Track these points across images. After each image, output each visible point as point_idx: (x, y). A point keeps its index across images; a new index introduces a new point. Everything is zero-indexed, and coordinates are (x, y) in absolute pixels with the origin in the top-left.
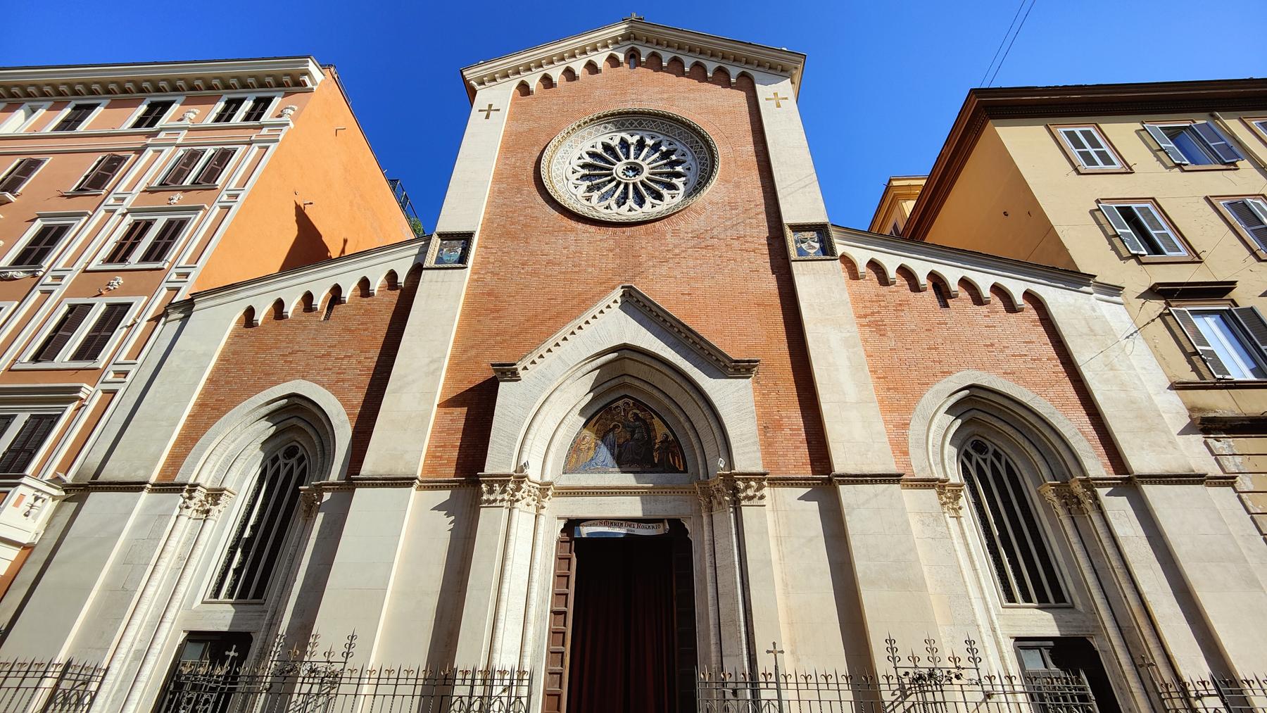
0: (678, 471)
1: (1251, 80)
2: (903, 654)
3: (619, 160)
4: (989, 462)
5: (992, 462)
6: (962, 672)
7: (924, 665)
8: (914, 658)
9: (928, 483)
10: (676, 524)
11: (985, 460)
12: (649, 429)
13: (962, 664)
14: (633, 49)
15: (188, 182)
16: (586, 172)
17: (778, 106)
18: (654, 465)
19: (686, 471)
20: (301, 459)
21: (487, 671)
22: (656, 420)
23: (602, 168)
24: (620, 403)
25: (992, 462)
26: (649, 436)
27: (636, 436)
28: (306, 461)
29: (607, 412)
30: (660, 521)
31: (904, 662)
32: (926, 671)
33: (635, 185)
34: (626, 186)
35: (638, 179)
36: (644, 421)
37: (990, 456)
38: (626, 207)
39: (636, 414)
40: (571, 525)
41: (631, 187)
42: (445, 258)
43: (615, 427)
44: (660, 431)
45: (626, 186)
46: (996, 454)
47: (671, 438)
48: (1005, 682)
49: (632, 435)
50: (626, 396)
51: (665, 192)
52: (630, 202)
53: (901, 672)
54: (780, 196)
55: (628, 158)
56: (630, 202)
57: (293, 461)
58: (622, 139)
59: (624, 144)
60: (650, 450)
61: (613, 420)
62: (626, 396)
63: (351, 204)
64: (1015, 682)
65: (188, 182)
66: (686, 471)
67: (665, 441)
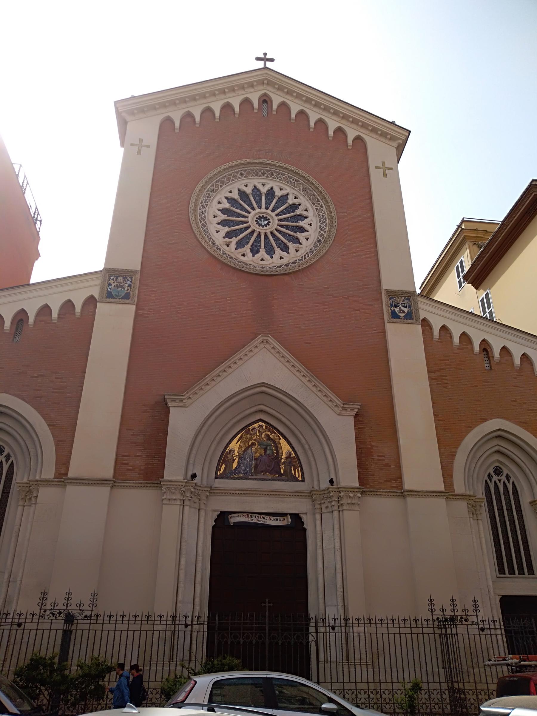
0: (297, 480)
2: (437, 607)
3: (260, 208)
4: (502, 482)
5: (504, 482)
6: (469, 618)
7: (449, 613)
8: (443, 610)
9: (189, 663)
10: (296, 517)
11: (500, 481)
12: (278, 447)
13: (469, 613)
14: (265, 95)
16: (225, 217)
17: (385, 175)
18: (281, 475)
19: (303, 481)
20: (8, 457)
21: (174, 617)
22: (283, 441)
23: (239, 215)
24: (256, 425)
25: (504, 482)
26: (277, 452)
27: (268, 452)
29: (246, 433)
30: (285, 515)
31: (438, 612)
32: (449, 617)
37: (503, 478)
39: (268, 435)
40: (223, 516)
43: (253, 444)
44: (285, 448)
46: (508, 477)
47: (293, 455)
48: (491, 623)
49: (265, 452)
50: (261, 420)
51: (291, 245)
53: (435, 617)
54: (128, 354)
55: (267, 208)
56: (262, 253)
60: (278, 463)
61: (251, 439)
62: (261, 420)
64: (496, 624)
66: (303, 481)
67: (289, 457)
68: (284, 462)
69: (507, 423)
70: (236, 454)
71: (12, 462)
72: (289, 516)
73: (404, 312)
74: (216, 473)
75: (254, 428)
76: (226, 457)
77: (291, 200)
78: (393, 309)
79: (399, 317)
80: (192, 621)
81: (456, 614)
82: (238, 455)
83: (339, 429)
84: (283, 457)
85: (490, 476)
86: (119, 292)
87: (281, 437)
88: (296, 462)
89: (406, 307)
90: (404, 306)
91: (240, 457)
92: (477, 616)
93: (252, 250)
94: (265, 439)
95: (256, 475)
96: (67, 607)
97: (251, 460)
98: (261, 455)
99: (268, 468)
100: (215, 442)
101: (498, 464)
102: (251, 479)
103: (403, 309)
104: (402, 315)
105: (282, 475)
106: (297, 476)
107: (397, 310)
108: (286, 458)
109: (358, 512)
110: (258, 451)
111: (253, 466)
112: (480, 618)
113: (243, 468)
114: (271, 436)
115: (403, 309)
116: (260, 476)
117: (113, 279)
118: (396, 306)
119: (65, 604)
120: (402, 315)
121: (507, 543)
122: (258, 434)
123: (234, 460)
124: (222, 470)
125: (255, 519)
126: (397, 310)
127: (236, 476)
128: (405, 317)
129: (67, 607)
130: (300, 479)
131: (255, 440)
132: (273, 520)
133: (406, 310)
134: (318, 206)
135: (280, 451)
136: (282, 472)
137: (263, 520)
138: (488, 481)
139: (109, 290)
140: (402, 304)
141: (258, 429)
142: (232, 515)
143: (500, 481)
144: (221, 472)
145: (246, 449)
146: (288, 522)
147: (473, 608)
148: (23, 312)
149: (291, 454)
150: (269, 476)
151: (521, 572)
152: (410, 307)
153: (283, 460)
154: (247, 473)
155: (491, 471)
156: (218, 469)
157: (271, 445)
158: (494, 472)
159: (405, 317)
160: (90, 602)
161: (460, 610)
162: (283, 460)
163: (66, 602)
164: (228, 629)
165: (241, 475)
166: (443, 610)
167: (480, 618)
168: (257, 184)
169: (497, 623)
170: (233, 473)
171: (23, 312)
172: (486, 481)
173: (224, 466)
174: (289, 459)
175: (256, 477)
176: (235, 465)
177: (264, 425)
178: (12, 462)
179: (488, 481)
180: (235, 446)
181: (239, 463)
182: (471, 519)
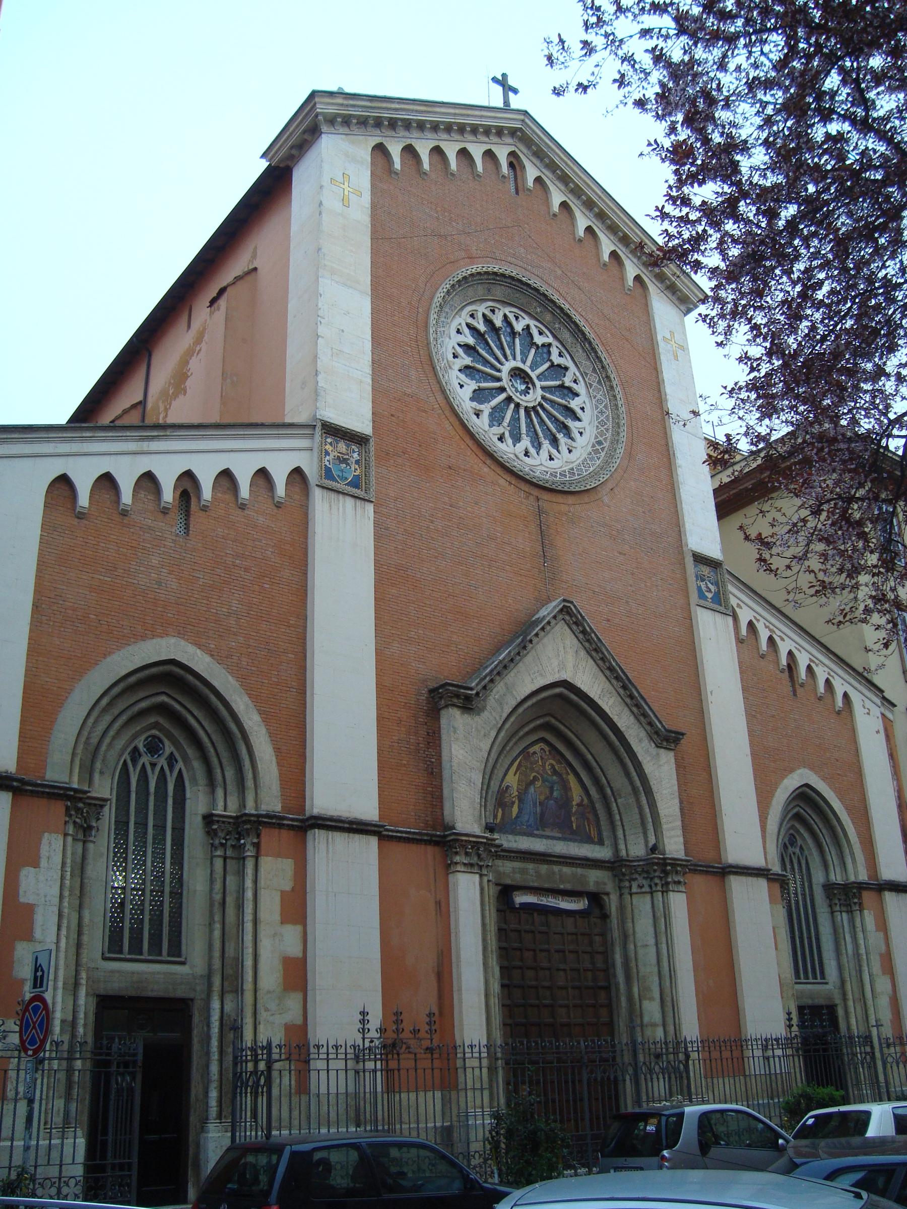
4: (158, 769)
10: (596, 899)
11: (153, 765)
12: (566, 788)
39: (553, 766)
69: (191, 649)
71: (180, 769)
81: (401, 1036)
85: (135, 754)
86: (342, 471)
101: (155, 732)
109: (684, 895)
113: (526, 818)
116: (548, 832)
117: (331, 444)
123: (513, 803)
134: (594, 382)
138: (166, 768)
141: (539, 754)
143: (153, 765)
147: (427, 1028)
148: (188, 476)
154: (530, 826)
155: (140, 744)
158: (145, 746)
164: (595, 1061)
168: (508, 314)
169: (476, 1050)
171: (188, 476)
175: (544, 833)
176: (515, 810)
177: (547, 749)
178: (180, 769)
179: (166, 768)
180: (512, 780)
182: (70, 839)
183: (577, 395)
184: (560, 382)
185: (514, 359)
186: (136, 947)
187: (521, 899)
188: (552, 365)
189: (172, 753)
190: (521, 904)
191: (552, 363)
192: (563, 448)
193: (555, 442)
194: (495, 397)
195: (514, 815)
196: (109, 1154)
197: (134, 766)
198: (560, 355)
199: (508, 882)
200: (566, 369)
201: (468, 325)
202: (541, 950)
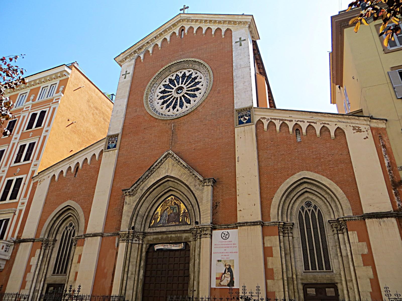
1: (332, 46)
4: (311, 211)
6: (253, 297)
11: (309, 210)
15: (4, 222)
22: (182, 205)
24: (169, 198)
27: (174, 211)
28: (75, 228)
33: (186, 93)
34: (186, 93)
35: (185, 91)
36: (177, 205)
37: (312, 208)
38: (184, 107)
39: (175, 202)
41: (185, 95)
42: (110, 146)
43: (168, 208)
45: (183, 96)
46: (315, 207)
47: (186, 211)
49: (173, 211)
52: (185, 104)
57: (71, 228)
58: (169, 79)
59: (171, 81)
61: (167, 205)
63: (93, 114)
65: (4, 222)
68: (182, 215)
70: (160, 214)
71: (319, 209)
72: (182, 244)
73: (246, 119)
74: (150, 225)
75: (169, 200)
76: (155, 216)
77: (187, 74)
78: (240, 119)
79: (243, 123)
80: (86, 298)
81: (245, 295)
82: (160, 215)
83: (205, 195)
84: (181, 213)
85: (303, 208)
87: (181, 202)
88: (188, 214)
89: (248, 116)
90: (246, 116)
91: (161, 216)
92: (258, 296)
93: (187, 103)
94: (173, 205)
95: (168, 224)
96: (244, 294)
97: (166, 217)
98: (171, 213)
99: (174, 220)
100: (285, 196)
102: (166, 226)
103: (246, 117)
104: (245, 121)
105: (181, 222)
106: (188, 222)
107: (242, 119)
108: (183, 213)
110: (169, 212)
111: (167, 219)
112: (260, 297)
113: (162, 221)
114: (176, 203)
115: (246, 117)
118: (242, 117)
119: (257, 293)
120: (245, 121)
121: (312, 250)
122: (170, 203)
123: (158, 217)
124: (153, 223)
125: (166, 247)
126: (242, 119)
127: (159, 225)
128: (247, 122)
129: (244, 294)
130: (189, 223)
131: (169, 206)
132: (175, 246)
133: (247, 118)
135: (180, 210)
136: (181, 221)
137: (170, 247)
138: (301, 211)
139: (109, 145)
140: (245, 115)
142: (156, 246)
144: (152, 224)
145: (164, 211)
146: (182, 247)
149: (185, 211)
150: (174, 223)
151: (321, 268)
152: (250, 115)
153: (181, 214)
154: (163, 223)
155: (304, 204)
156: (151, 223)
157: (176, 207)
159: (247, 122)
160: (256, 291)
161: (248, 293)
162: (181, 214)
163: (244, 291)
165: (161, 225)
166: (251, 293)
167: (260, 297)
170: (157, 224)
172: (300, 211)
173: (154, 221)
174: (184, 214)
175: (168, 225)
177: (173, 197)
178: (319, 209)
181: (160, 219)
183: (185, 73)
184: (181, 78)
185: (171, 92)
186: (314, 268)
187: (157, 247)
188: (175, 79)
189: (315, 205)
190: (157, 249)
191: (174, 79)
192: (200, 80)
193: (199, 83)
194: (177, 102)
195: (158, 222)
196: (63, 272)
197: (303, 211)
198: (173, 76)
199: (151, 243)
200: (177, 75)
201: (198, 76)
202: (179, 268)
